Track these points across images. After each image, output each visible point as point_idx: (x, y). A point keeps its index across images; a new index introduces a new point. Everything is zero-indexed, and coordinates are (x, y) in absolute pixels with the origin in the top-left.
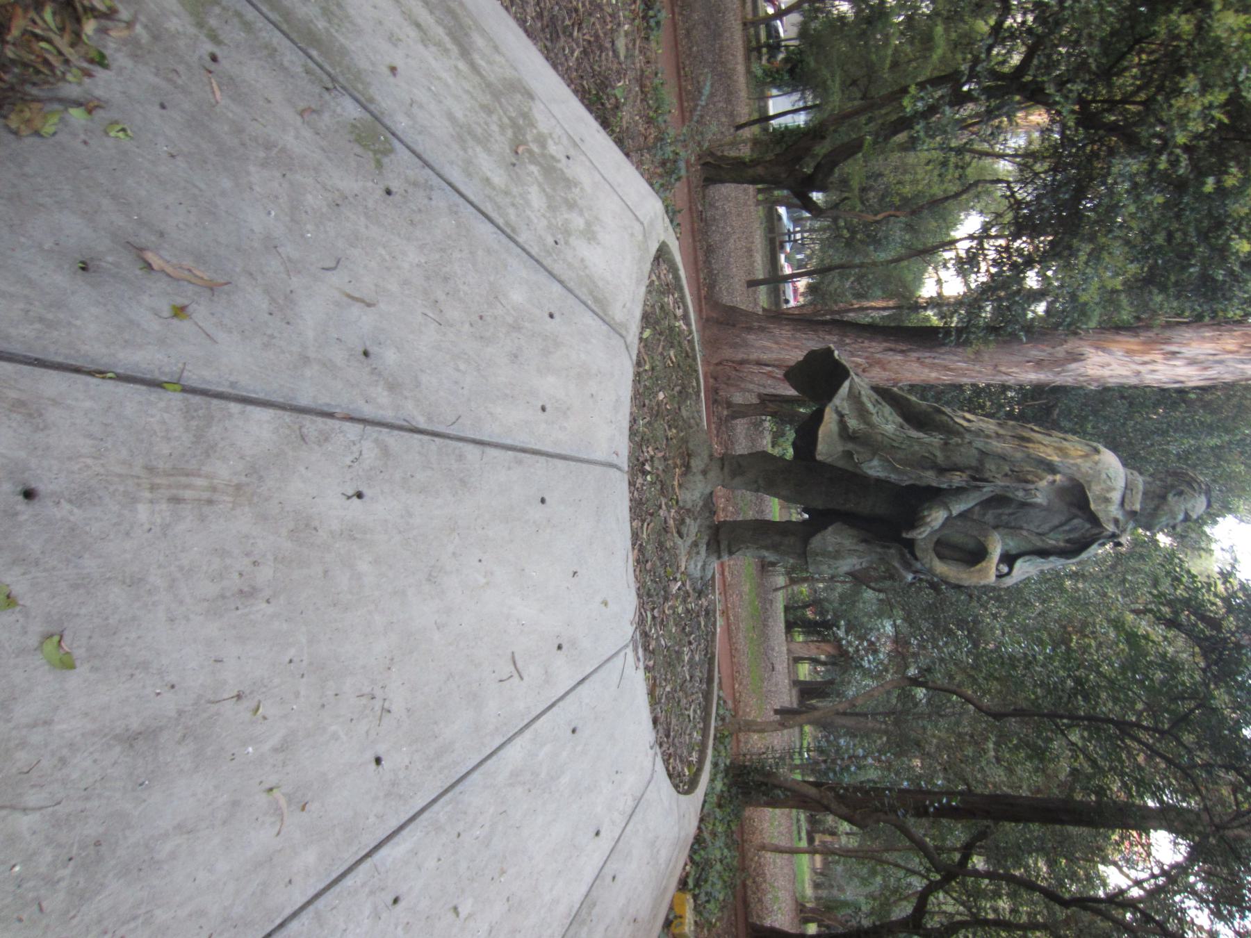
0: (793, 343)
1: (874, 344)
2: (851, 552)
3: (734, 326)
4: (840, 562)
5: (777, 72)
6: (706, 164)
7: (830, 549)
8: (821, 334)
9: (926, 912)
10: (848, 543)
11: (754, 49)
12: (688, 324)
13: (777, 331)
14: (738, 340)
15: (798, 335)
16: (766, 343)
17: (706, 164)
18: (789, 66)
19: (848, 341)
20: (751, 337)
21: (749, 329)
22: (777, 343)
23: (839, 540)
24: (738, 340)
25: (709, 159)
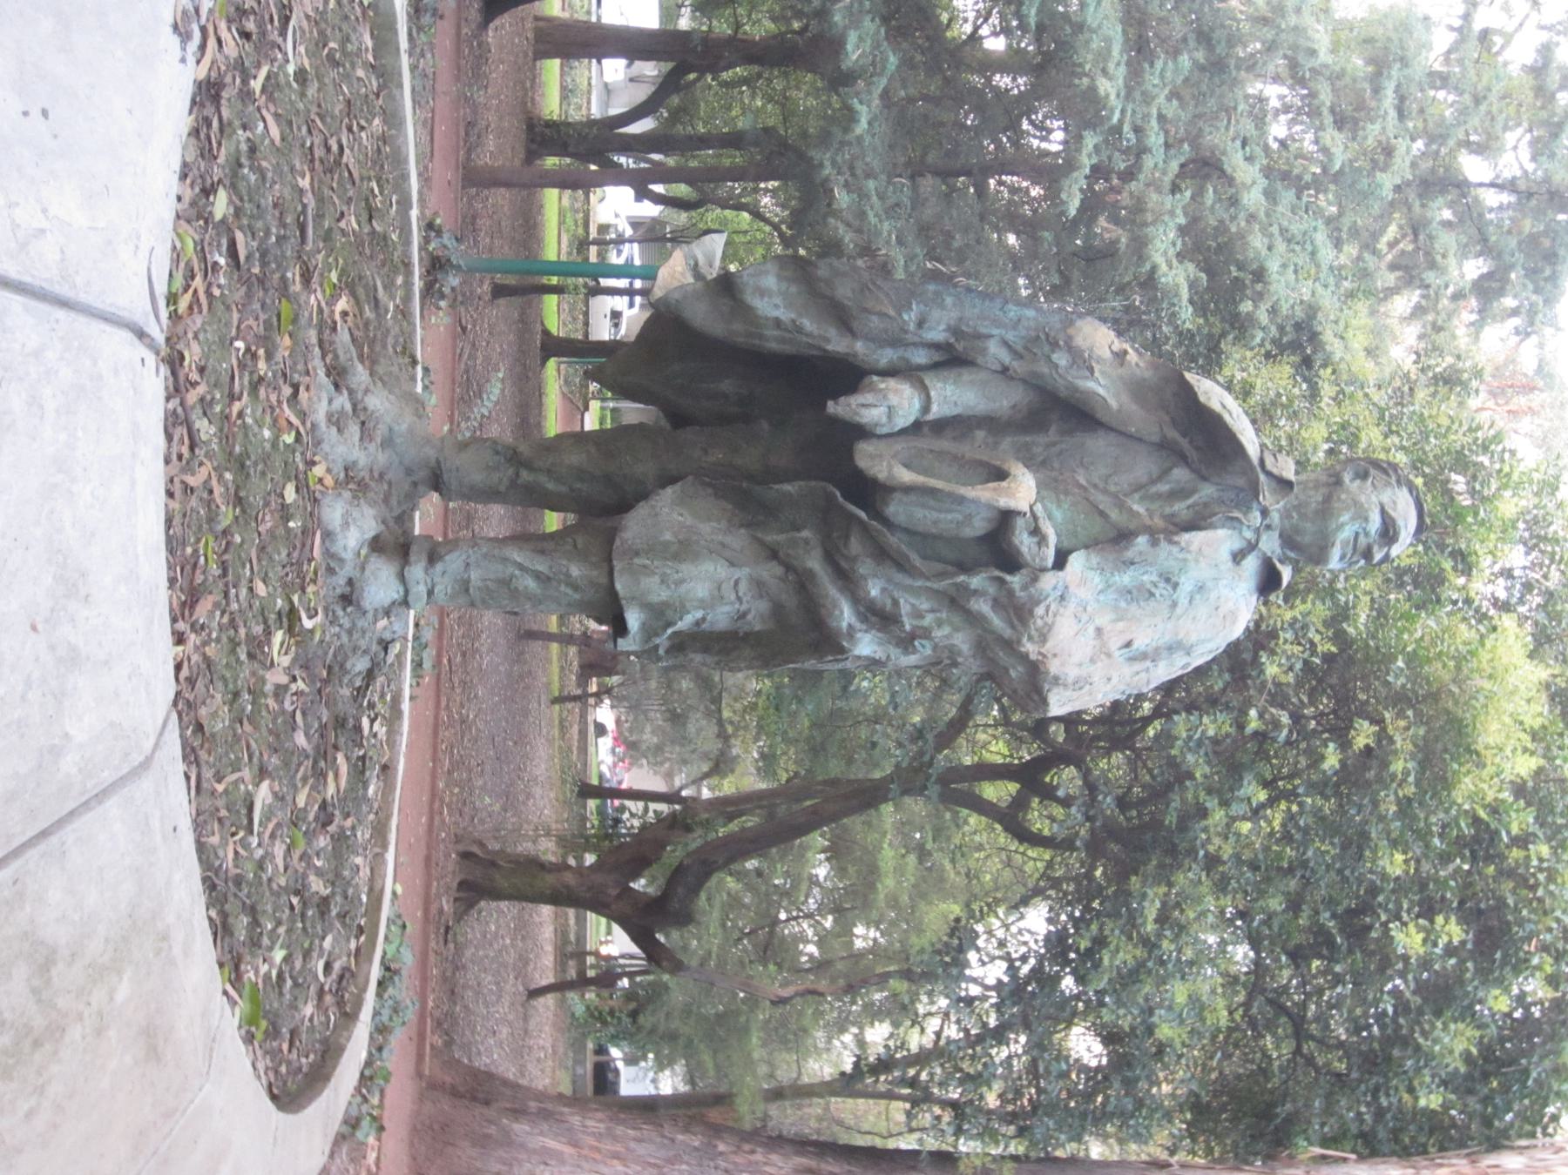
0: (607, 1146)
1: (774, 1157)
2: (719, 551)
3: (487, 1103)
4: (687, 569)
5: (612, 1013)
6: (466, 856)
7: (668, 536)
8: (668, 1130)
9: (877, 809)
10: (709, 530)
11: (572, 955)
12: (393, 732)
13: (576, 1120)
14: (492, 1130)
15: (620, 1130)
16: (552, 1144)
17: (466, 856)
18: (633, 1005)
19: (722, 1147)
20: (520, 1128)
21: (518, 1113)
22: (575, 1144)
23: (689, 521)
24: (492, 1130)
25: (475, 849)
